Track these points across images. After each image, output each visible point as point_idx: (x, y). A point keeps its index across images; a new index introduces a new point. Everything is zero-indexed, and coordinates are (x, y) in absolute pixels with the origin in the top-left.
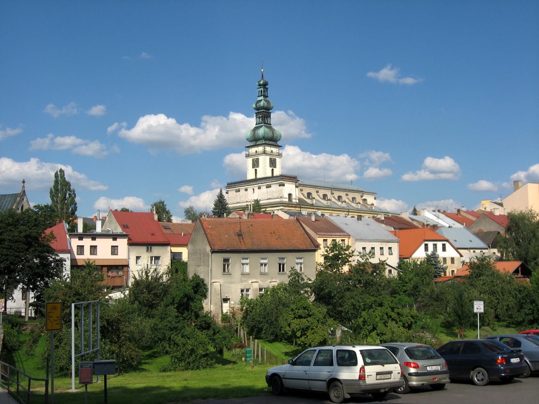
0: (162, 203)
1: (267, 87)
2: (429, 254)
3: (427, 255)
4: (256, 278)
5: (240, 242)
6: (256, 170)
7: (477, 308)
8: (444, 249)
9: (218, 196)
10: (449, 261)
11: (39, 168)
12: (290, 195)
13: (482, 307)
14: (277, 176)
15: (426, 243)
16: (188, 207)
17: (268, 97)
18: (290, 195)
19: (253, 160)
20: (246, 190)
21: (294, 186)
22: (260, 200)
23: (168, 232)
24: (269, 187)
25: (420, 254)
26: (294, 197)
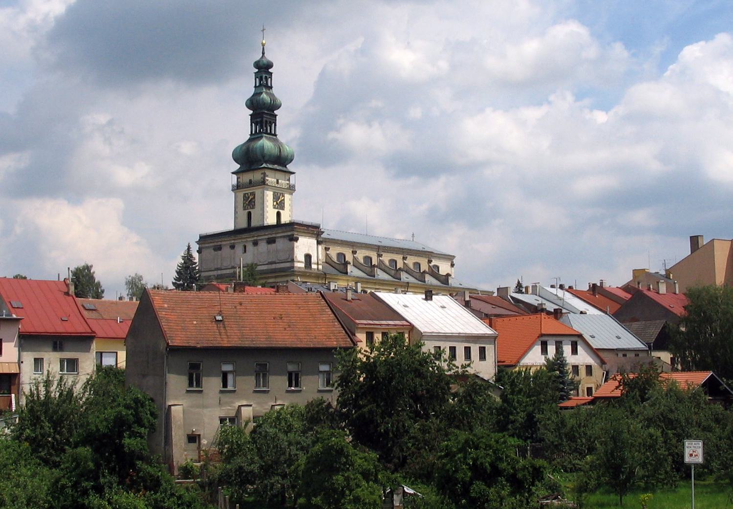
0: (88, 268)
1: (270, 70)
2: (551, 358)
3: (548, 360)
4: (247, 399)
5: (220, 334)
6: (249, 214)
7: (691, 455)
8: (574, 351)
9: (184, 258)
10: (583, 371)
11: (244, 421)
12: (308, 257)
13: (700, 451)
14: (286, 225)
15: (544, 339)
16: (134, 275)
17: (271, 87)
18: (308, 257)
19: (245, 194)
20: (232, 247)
21: (315, 242)
22: (257, 265)
23: (93, 315)
24: (271, 241)
25: (535, 359)
26: (314, 259)
